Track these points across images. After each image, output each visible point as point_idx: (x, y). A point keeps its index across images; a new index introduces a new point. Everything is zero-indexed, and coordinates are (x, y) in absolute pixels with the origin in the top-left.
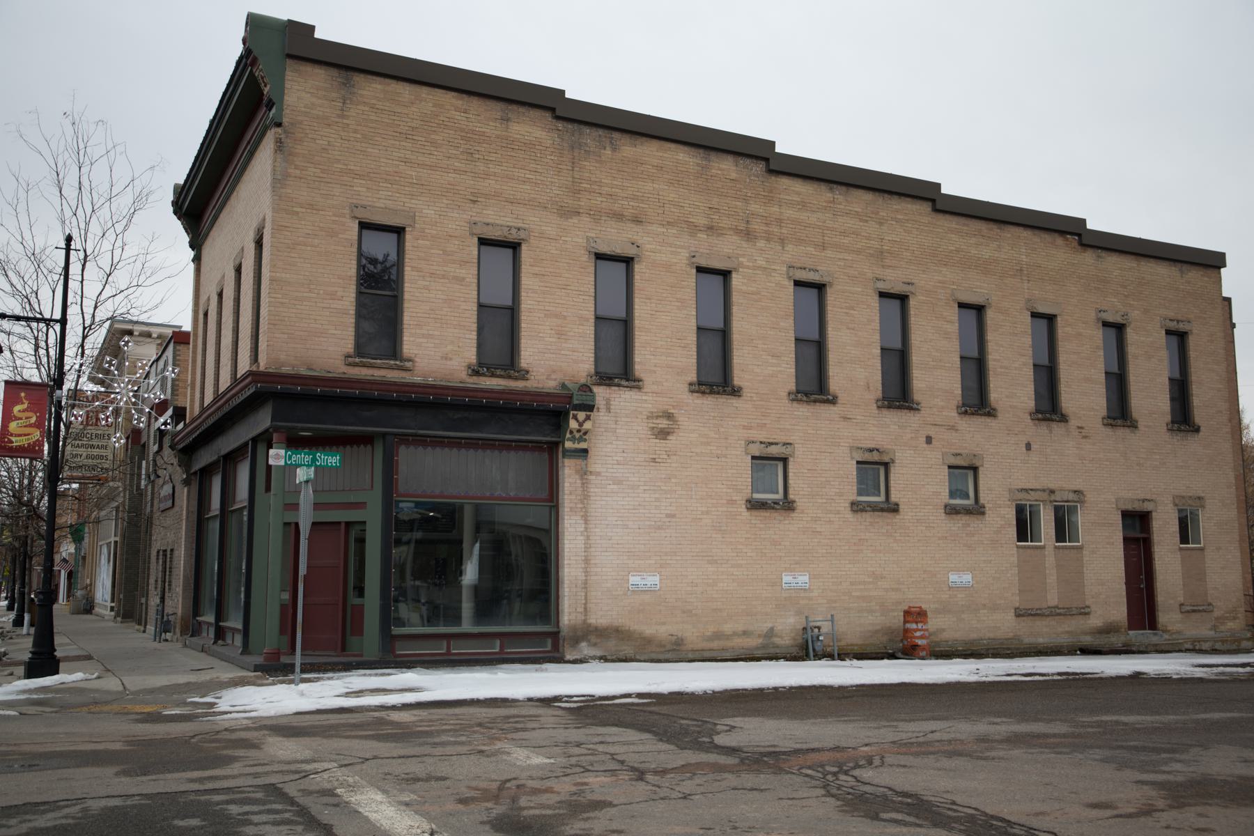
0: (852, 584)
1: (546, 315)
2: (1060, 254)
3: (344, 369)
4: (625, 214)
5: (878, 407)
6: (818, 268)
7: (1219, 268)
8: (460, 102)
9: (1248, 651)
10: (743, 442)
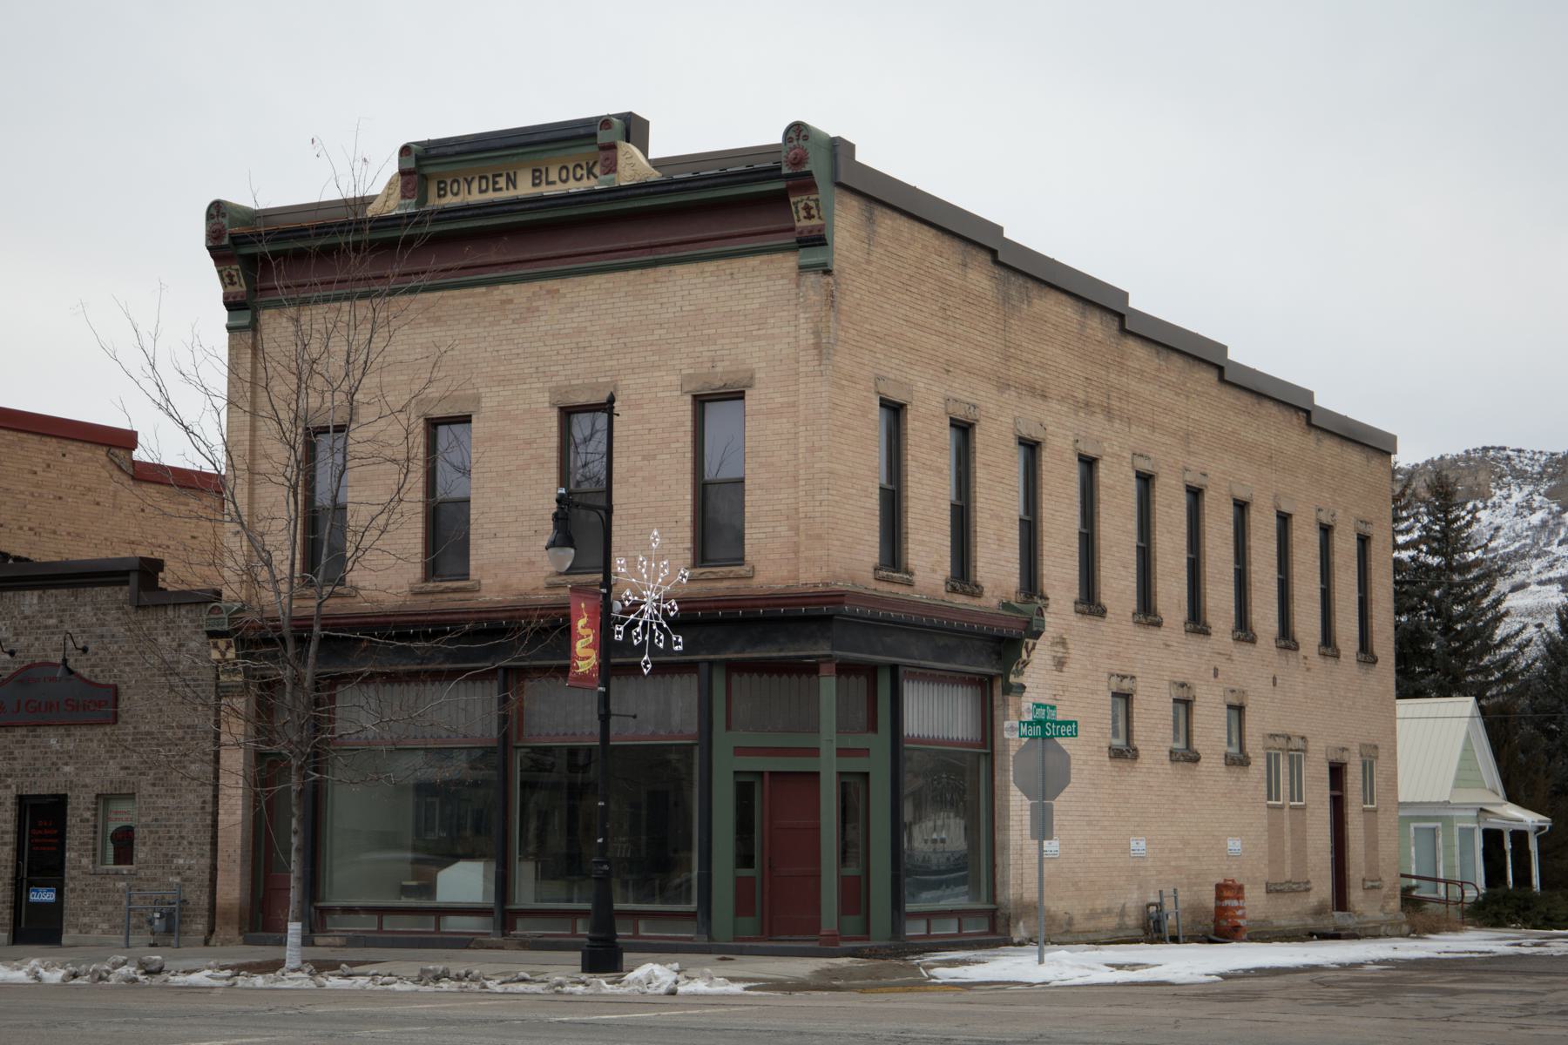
0: (1171, 851)
1: (991, 516)
2: (1290, 437)
3: (873, 584)
4: (1037, 387)
5: (1186, 631)
6: (1151, 455)
7: (1389, 454)
8: (937, 242)
9: (1566, 928)
10: (1106, 675)
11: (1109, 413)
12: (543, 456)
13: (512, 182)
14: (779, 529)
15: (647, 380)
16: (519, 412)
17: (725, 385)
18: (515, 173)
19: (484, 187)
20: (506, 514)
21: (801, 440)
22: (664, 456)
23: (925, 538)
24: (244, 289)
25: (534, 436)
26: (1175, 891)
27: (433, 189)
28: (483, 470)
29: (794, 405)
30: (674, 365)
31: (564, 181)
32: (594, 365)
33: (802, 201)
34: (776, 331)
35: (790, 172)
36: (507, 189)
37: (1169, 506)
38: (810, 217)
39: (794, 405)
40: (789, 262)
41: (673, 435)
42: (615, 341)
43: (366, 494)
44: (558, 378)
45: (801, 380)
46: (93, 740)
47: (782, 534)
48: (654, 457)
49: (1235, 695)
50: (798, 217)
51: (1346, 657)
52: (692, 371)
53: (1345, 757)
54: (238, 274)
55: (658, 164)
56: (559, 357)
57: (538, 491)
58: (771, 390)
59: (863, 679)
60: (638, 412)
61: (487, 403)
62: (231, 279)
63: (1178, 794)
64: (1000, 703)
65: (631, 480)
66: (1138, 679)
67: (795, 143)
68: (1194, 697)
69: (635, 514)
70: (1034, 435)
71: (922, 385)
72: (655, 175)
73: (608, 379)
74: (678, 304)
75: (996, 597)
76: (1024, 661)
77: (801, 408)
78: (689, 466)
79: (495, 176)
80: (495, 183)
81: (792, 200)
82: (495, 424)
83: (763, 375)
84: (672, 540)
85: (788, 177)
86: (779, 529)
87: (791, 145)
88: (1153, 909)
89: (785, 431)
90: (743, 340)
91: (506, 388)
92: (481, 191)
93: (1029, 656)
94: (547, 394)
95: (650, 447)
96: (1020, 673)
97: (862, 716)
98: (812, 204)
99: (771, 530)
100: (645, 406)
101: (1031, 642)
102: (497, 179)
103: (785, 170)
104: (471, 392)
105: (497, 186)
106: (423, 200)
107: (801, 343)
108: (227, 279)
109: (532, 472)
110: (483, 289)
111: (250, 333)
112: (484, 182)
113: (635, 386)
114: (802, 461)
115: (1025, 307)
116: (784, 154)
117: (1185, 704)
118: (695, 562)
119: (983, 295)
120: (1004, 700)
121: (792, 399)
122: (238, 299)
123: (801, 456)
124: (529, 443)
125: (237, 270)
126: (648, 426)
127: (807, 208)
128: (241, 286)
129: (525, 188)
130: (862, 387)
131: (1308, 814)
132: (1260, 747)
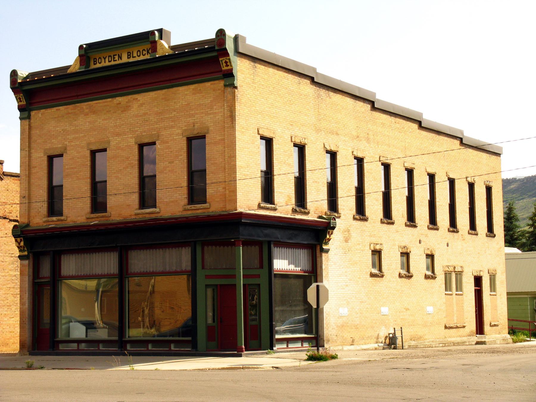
11: (368, 140)
12: (133, 163)
13: (120, 57)
14: (219, 189)
15: (169, 132)
16: (124, 146)
17: (198, 133)
18: (121, 54)
19: (110, 60)
20: (120, 186)
21: (226, 153)
22: (177, 162)
23: (282, 191)
24: (25, 103)
25: (129, 156)
26: (401, 328)
27: (92, 62)
28: (111, 170)
29: (224, 140)
30: (180, 126)
31: (139, 56)
32: (150, 127)
33: (224, 59)
34: (217, 111)
35: (218, 48)
36: (118, 60)
37: (397, 176)
38: (227, 66)
39: (224, 140)
40: (221, 83)
41: (180, 153)
42: (158, 117)
43: (70, 180)
44: (138, 133)
45: (226, 130)
46: (207, 274)
47: (220, 191)
48: (173, 162)
49: (429, 250)
50: (223, 66)
51: (481, 234)
52: (186, 128)
53: (482, 274)
54: (22, 98)
55: (173, 48)
56: (138, 125)
57: (131, 177)
58: (215, 134)
59: (257, 247)
60: (167, 145)
61: (113, 143)
62: (20, 100)
63: (403, 290)
64: (319, 255)
65: (165, 171)
66: (384, 245)
67: (220, 37)
68: (410, 252)
69: (166, 185)
70: (333, 149)
71: (280, 131)
72: (171, 52)
73: (156, 132)
74: (181, 102)
75: (317, 214)
76: (328, 239)
77: (226, 141)
78: (185, 165)
79: (114, 55)
80: (114, 58)
81: (220, 59)
82: (115, 151)
83: (212, 129)
84: (180, 195)
85: (217, 50)
86: (219, 189)
87: (219, 38)
88: (391, 335)
89: (221, 150)
90: (204, 115)
91: (119, 137)
92: (109, 62)
93: (330, 237)
94: (134, 139)
95: (171, 158)
96: (326, 244)
97: (257, 262)
98: (227, 60)
99: (216, 189)
100: (169, 142)
101: (331, 231)
102: (115, 57)
103: (217, 48)
104: (106, 139)
105: (115, 59)
106: (88, 65)
107: (225, 115)
108: (19, 100)
109: (129, 169)
110: (110, 99)
111: (28, 120)
112: (110, 58)
113: (165, 135)
114: (226, 162)
115: (328, 99)
116: (216, 41)
117: (406, 255)
118: (189, 202)
119: (308, 95)
120: (320, 254)
121: (223, 137)
122: (23, 107)
123: (226, 160)
124: (128, 158)
125: (22, 96)
126: (170, 150)
127: (226, 62)
128: (24, 102)
129: (125, 59)
130: (252, 132)
131: (464, 297)
132: (442, 271)
